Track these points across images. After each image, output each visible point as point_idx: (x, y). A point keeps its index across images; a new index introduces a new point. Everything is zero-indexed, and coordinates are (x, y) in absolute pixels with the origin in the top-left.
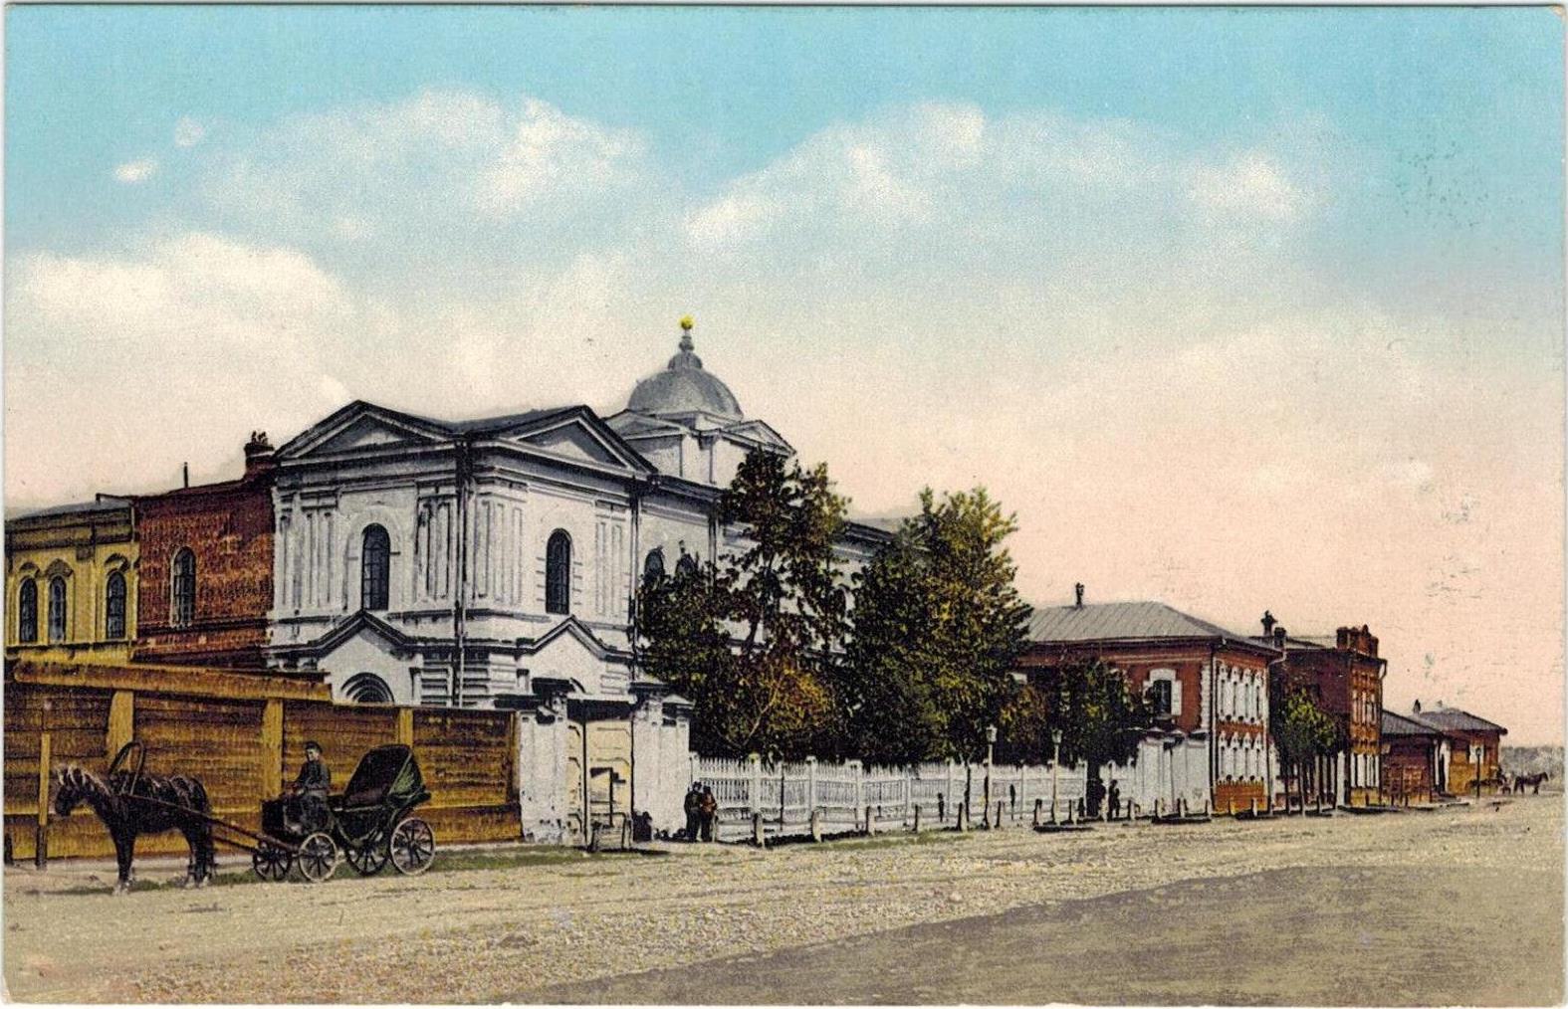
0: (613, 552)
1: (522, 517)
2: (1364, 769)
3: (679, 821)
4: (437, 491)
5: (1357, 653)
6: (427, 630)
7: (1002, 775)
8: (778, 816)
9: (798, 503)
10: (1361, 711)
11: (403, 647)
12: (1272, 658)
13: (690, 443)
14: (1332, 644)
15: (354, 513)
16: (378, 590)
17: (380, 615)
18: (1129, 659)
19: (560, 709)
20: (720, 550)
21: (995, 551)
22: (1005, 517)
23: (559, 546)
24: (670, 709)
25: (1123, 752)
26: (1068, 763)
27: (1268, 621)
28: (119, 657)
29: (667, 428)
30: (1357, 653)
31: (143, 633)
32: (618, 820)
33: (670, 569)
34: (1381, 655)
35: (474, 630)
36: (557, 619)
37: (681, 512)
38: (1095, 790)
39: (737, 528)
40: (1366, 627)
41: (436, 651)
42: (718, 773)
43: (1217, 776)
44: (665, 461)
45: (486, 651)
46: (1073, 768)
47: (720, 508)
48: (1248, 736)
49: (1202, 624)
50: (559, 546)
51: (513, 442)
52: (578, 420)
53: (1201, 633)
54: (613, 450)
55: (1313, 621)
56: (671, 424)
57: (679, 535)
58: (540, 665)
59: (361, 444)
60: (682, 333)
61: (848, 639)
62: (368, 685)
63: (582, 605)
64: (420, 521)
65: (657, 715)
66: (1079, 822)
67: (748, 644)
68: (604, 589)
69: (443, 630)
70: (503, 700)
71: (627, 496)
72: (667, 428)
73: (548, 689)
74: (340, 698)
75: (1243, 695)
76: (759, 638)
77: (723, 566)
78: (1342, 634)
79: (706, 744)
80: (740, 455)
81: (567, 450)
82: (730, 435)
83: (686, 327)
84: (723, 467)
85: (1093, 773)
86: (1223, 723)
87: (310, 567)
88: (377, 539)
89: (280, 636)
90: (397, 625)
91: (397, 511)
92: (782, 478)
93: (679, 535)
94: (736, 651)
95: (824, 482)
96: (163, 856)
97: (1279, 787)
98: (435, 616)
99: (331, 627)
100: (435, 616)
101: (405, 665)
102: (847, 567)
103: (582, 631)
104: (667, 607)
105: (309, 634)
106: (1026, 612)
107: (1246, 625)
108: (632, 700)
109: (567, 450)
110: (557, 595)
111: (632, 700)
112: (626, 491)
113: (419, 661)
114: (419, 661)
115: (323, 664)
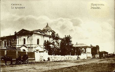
0: (42, 40)
1: (35, 37)
2: (98, 56)
3: (47, 60)
5: (97, 47)
6: (28, 46)
7: (72, 56)
9: (56, 36)
10: (98, 51)
11: (26, 47)
13: (48, 32)
15: (23, 38)
16: (24, 43)
17: (25, 45)
18: (81, 48)
19: (38, 52)
20: (51, 40)
21: (70, 40)
22: (71, 37)
23: (38, 40)
24: (46, 52)
25: (80, 54)
26: (76, 55)
27: (91, 45)
28: (5, 48)
30: (97, 47)
31: (7, 46)
32: (43, 60)
33: (46, 41)
35: (32, 46)
36: (38, 45)
38: (78, 58)
39: (51, 38)
41: (29, 47)
42: (50, 56)
44: (46, 33)
45: (33, 48)
47: (50, 37)
50: (38, 40)
51: (35, 32)
52: (39, 31)
54: (43, 33)
55: (94, 45)
57: (47, 39)
58: (37, 49)
59: (24, 33)
61: (60, 46)
62: (24, 50)
63: (40, 44)
64: (28, 38)
65: (46, 52)
67: (52, 47)
68: (42, 43)
69: (29, 46)
70: (34, 51)
73: (37, 50)
74: (22, 51)
75: (89, 50)
76: (53, 46)
77: (50, 41)
79: (49, 54)
80: (52, 33)
81: (39, 33)
82: (51, 31)
84: (50, 34)
85: (78, 56)
87: (20, 42)
88: (24, 40)
89: (17, 47)
90: (26, 46)
91: (26, 38)
92: (55, 35)
93: (47, 39)
94: (51, 47)
95: (58, 35)
96: (8, 63)
97: (92, 57)
98: (29, 45)
99: (21, 46)
100: (29, 45)
101: (27, 48)
102: (60, 41)
103: (40, 46)
104: (47, 45)
105: (20, 46)
106: (73, 45)
107: (89, 45)
108: (44, 51)
109: (39, 33)
111: (44, 51)
113: (28, 48)
114: (28, 48)
115: (20, 49)
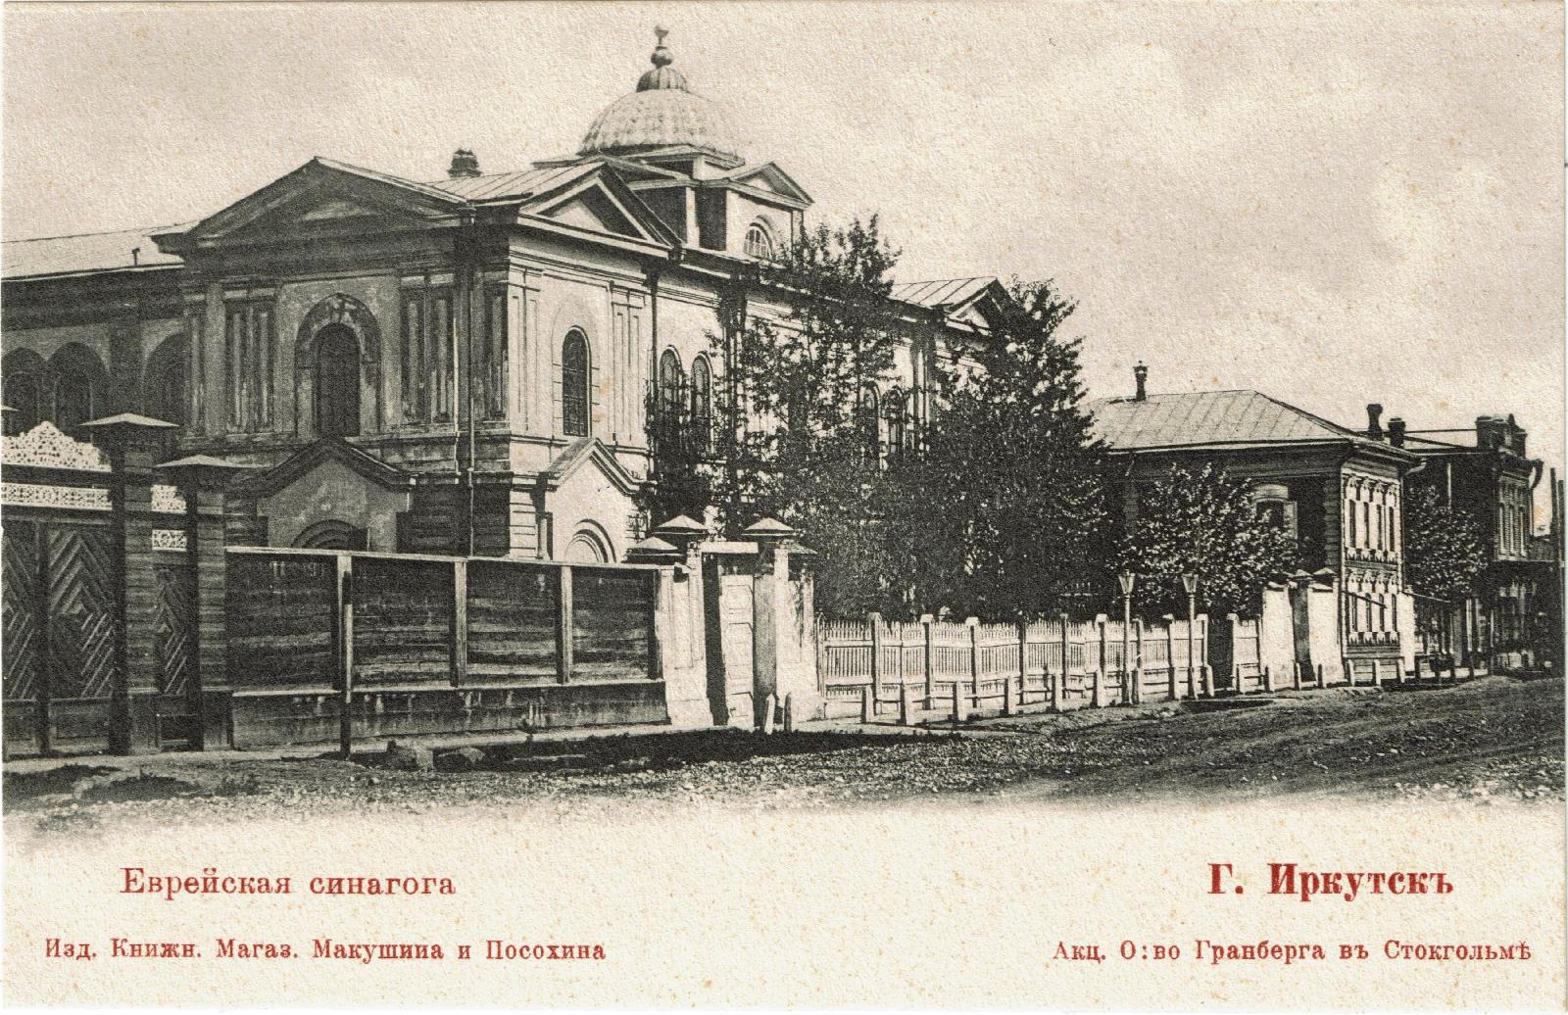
4: (427, 279)
8: (1049, 704)
12: (1408, 467)
14: (1470, 440)
23: (576, 348)
29: (653, 177)
34: (1531, 454)
37: (680, 289)
40: (1511, 417)
43: (1348, 632)
46: (265, 519)
48: (1368, 575)
49: (1329, 425)
50: (576, 348)
53: (1320, 433)
56: (660, 171)
60: (655, 40)
66: (1217, 694)
71: (644, 277)
72: (653, 177)
78: (1483, 425)
83: (661, 33)
86: (1352, 559)
110: (577, 411)
112: (643, 272)
